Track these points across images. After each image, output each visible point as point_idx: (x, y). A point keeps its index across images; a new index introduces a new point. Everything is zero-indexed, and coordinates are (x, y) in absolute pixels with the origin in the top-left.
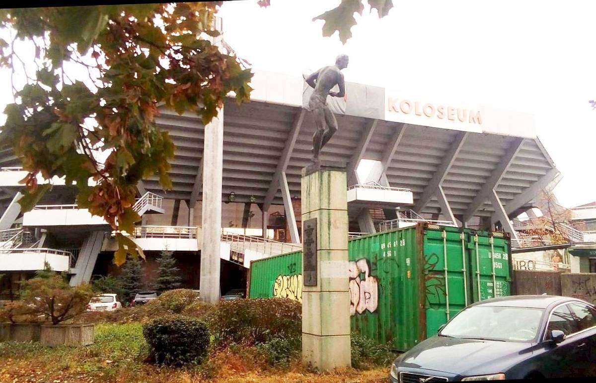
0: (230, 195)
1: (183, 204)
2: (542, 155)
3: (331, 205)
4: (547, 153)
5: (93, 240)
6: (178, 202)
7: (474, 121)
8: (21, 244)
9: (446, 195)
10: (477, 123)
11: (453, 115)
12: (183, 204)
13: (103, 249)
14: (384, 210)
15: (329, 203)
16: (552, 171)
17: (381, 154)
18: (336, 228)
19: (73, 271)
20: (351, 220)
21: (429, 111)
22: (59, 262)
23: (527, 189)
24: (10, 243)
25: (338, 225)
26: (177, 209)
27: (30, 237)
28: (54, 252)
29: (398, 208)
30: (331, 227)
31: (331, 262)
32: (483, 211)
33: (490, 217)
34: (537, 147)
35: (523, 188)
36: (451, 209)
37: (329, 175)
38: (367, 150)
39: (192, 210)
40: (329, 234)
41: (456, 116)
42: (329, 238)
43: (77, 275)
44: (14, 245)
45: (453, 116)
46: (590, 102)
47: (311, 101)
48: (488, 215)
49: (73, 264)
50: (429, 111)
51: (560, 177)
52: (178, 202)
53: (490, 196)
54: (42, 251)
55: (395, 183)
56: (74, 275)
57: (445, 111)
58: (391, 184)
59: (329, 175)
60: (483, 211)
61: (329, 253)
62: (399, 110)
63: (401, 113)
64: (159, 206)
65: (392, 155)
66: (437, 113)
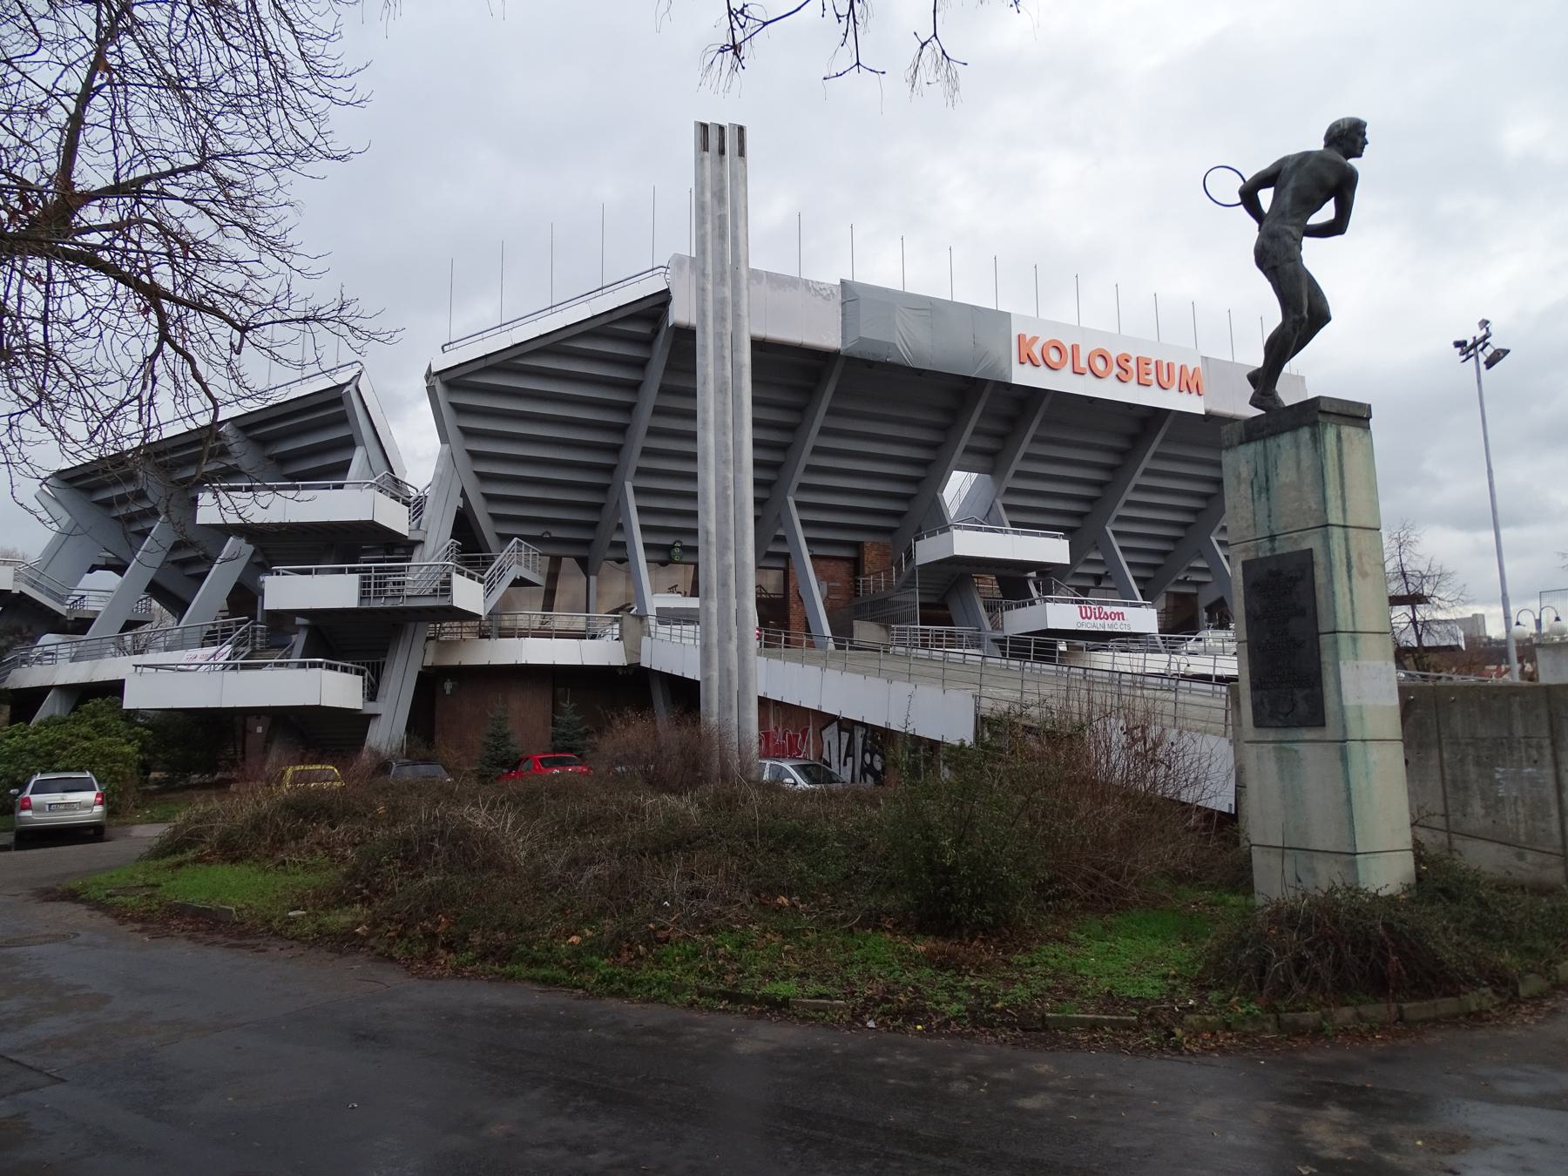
0: (673, 547)
1: (569, 565)
3: (1349, 513)
5: (409, 637)
6: (556, 561)
8: (248, 650)
9: (1122, 549)
12: (569, 565)
13: (428, 662)
14: (1000, 580)
15: (1344, 511)
17: (990, 460)
18: (1364, 575)
19: (371, 708)
21: (1054, 356)
22: (338, 688)
24: (227, 649)
25: (1368, 568)
26: (553, 577)
28: (335, 668)
29: (1033, 574)
30: (1354, 571)
31: (1360, 663)
32: (1184, 582)
37: (1339, 437)
38: (968, 450)
39: (593, 579)
40: (1351, 591)
41: (1152, 377)
42: (1352, 601)
43: (383, 718)
44: (235, 655)
46: (1458, 344)
47: (1268, 243)
48: (1192, 590)
49: (372, 693)
50: (1054, 356)
52: (556, 561)
53: (1206, 552)
54: (302, 665)
55: (1026, 521)
56: (377, 716)
57: (1132, 364)
58: (1013, 524)
59: (1339, 437)
60: (1184, 582)
61: (1354, 641)
62: (1041, 361)
63: (1043, 367)
64: (534, 570)
65: (1017, 464)
66: (1116, 370)
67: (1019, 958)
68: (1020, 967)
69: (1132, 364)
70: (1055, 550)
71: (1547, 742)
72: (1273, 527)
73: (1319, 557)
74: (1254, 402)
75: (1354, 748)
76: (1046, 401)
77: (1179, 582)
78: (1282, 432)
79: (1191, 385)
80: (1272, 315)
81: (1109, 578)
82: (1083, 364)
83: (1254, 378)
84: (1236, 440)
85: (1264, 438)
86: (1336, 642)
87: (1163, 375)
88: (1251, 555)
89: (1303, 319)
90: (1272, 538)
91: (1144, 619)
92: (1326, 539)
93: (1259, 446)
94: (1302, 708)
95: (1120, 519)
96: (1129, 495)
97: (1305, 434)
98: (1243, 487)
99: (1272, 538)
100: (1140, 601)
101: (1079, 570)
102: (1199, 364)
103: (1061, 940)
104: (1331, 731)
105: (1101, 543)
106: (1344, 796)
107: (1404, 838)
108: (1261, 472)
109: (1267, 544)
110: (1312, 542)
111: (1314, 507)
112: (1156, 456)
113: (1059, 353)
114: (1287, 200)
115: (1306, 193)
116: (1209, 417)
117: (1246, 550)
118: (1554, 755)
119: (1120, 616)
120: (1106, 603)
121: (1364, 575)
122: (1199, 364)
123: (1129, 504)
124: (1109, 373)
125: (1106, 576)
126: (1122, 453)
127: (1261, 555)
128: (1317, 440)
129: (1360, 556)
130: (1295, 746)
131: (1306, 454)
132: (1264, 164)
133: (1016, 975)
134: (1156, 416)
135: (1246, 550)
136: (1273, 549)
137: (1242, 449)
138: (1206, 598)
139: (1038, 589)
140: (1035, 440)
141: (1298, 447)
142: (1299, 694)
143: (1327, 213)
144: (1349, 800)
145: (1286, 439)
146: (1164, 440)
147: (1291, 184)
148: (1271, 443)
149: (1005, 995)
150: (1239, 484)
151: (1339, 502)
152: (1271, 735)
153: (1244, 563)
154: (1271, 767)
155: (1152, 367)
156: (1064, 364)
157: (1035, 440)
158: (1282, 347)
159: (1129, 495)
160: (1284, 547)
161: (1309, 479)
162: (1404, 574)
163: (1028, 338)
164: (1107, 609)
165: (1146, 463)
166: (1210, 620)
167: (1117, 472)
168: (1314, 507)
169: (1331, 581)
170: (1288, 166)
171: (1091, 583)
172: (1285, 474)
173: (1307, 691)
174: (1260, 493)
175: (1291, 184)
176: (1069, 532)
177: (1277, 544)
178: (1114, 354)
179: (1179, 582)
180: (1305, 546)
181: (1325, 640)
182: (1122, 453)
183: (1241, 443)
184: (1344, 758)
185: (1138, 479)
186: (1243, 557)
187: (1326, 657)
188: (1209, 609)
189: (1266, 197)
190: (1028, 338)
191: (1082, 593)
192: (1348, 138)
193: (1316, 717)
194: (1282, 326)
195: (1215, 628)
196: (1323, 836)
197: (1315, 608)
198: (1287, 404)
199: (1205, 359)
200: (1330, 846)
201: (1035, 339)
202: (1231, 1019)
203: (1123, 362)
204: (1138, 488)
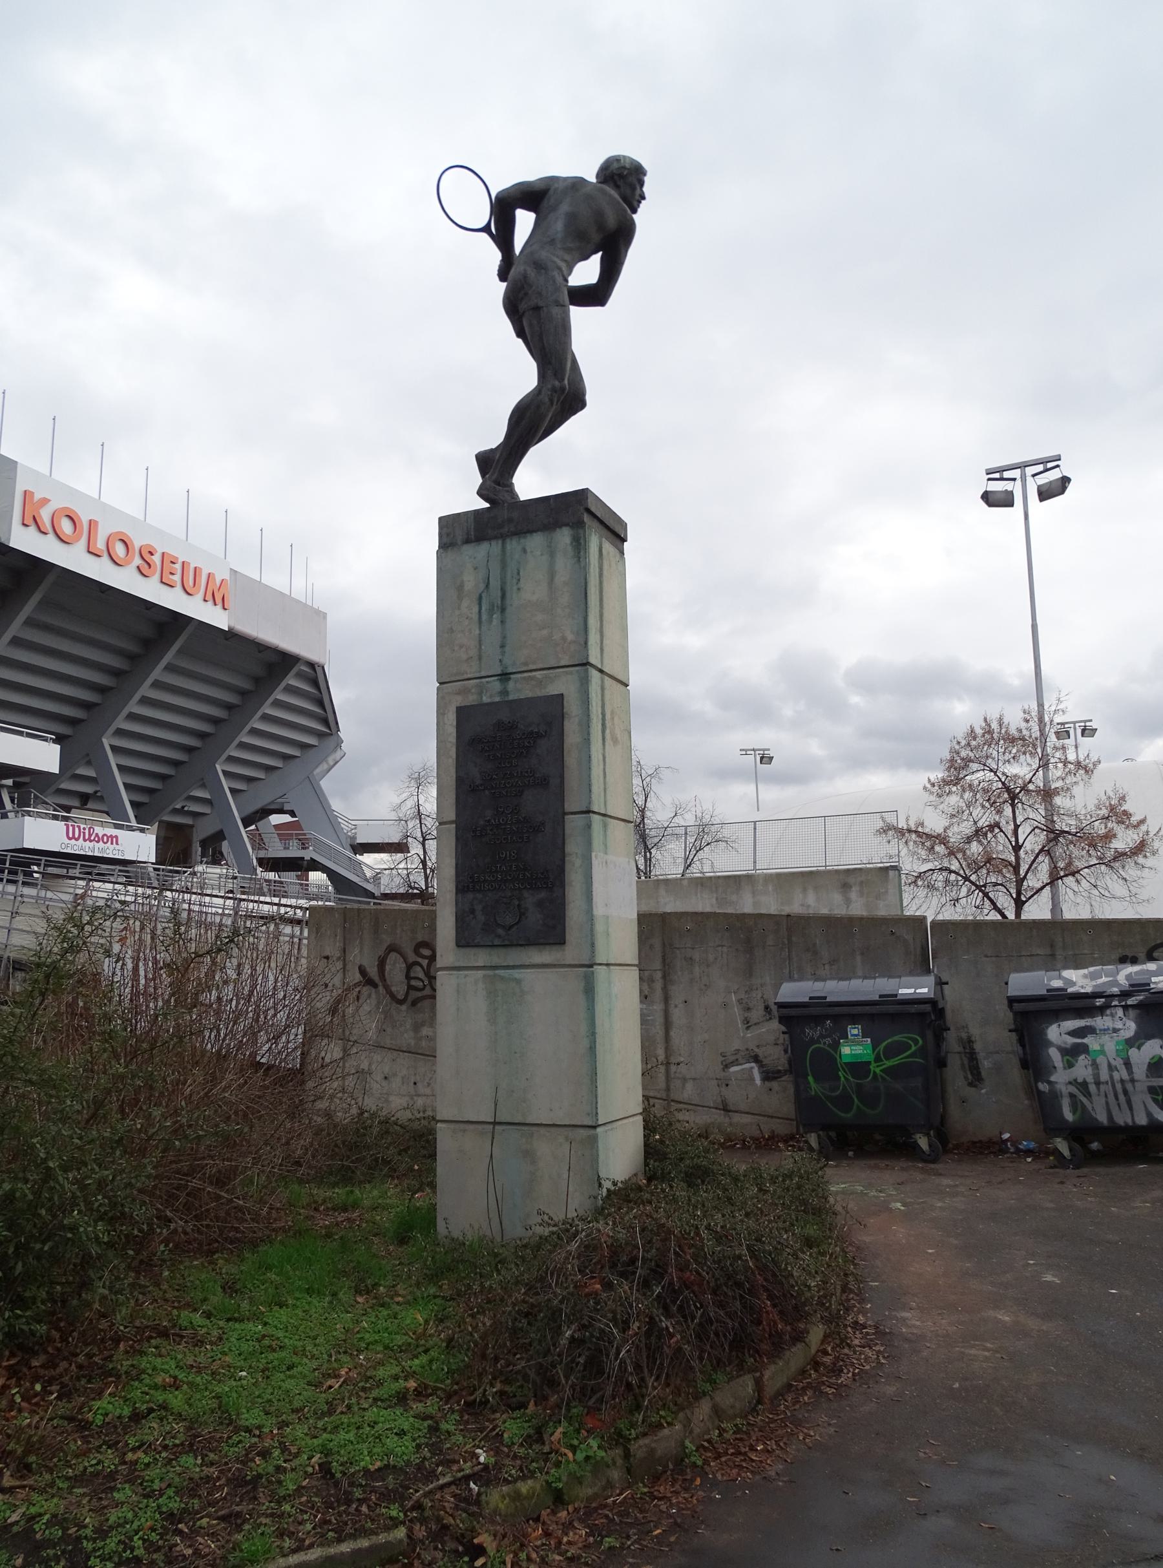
2: (320, 703)
4: (593, 945)
7: (972, 1056)
9: (119, 767)
10: (220, 606)
11: (172, 574)
16: (331, 742)
20: (445, 540)
21: (66, 527)
23: (278, 772)
27: (490, 621)
31: (610, 858)
32: (181, 811)
33: (192, 826)
34: (315, 683)
35: (269, 769)
36: (124, 784)
41: (177, 578)
45: (171, 577)
48: (187, 821)
50: (66, 527)
51: (338, 754)
53: (208, 780)
57: (156, 559)
60: (181, 811)
63: (51, 536)
66: (138, 561)
67: (107, 1406)
68: (113, 1433)
69: (156, 559)
70: (42, 755)
71: (659, 975)
72: (507, 661)
73: (572, 706)
74: (482, 493)
75: (600, 971)
76: (50, 579)
77: (175, 811)
78: (531, 532)
79: (217, 597)
80: (521, 374)
81: (101, 799)
82: (101, 545)
83: (485, 461)
84: (459, 540)
85: (503, 537)
86: (589, 826)
87: (188, 578)
88: (471, 699)
89: (563, 389)
90: (504, 676)
91: (139, 845)
92: (585, 682)
93: (495, 547)
94: (534, 918)
95: (120, 733)
96: (133, 707)
97: (564, 537)
98: (465, 603)
99: (504, 676)
100: (134, 823)
101: (63, 786)
102: (227, 576)
103: (164, 1334)
104: (571, 953)
105: (94, 757)
106: (586, 1043)
107: (635, 1103)
108: (495, 583)
109: (496, 685)
110: (564, 685)
111: (570, 637)
112: (170, 668)
113: (70, 524)
114: (558, 226)
115: (564, 240)
116: (231, 636)
117: (463, 692)
118: (665, 989)
119: (114, 839)
120: (102, 824)
121: (615, 741)
122: (227, 576)
123: (132, 717)
124: (128, 563)
125: (94, 796)
126: (132, 658)
127: (486, 699)
128: (579, 545)
129: (612, 713)
130: (516, 974)
131: (564, 565)
132: (530, 173)
133: (109, 1459)
134: (174, 622)
135: (463, 692)
136: (505, 692)
137: (468, 550)
138: (203, 830)
139: (12, 801)
140: (30, 623)
141: (552, 554)
142: (530, 899)
143: (586, 272)
144: (592, 1049)
145: (536, 542)
146: (179, 651)
147: (565, 208)
148: (513, 545)
149: (102, 1533)
150: (460, 598)
151: (598, 636)
152: (482, 957)
153: (460, 710)
154: (478, 1004)
155: (178, 566)
156: (78, 539)
157: (30, 623)
158: (533, 421)
159: (133, 707)
160: (520, 690)
161: (565, 599)
162: (419, 814)
163: (37, 497)
164: (99, 830)
165: (157, 673)
166: (203, 856)
167: (123, 677)
168: (570, 637)
169: (587, 741)
170: (561, 185)
171: (76, 803)
172: (531, 588)
173: (543, 895)
174: (491, 612)
175: (565, 208)
176: (59, 739)
177: (511, 685)
178: (137, 543)
179: (175, 811)
180: (553, 690)
181: (573, 823)
182: (132, 658)
183: (467, 541)
184: (589, 990)
185: (146, 690)
186: (459, 701)
187: (573, 847)
188: (204, 843)
189: (525, 221)
190: (37, 497)
191: (62, 812)
192: (624, 180)
193: (552, 932)
194: (537, 391)
195: (207, 863)
196: (549, 1103)
197: (562, 777)
198: (522, 498)
199: (234, 572)
200: (560, 1117)
201: (45, 501)
202: (559, 1476)
203: (146, 554)
204: (145, 701)
